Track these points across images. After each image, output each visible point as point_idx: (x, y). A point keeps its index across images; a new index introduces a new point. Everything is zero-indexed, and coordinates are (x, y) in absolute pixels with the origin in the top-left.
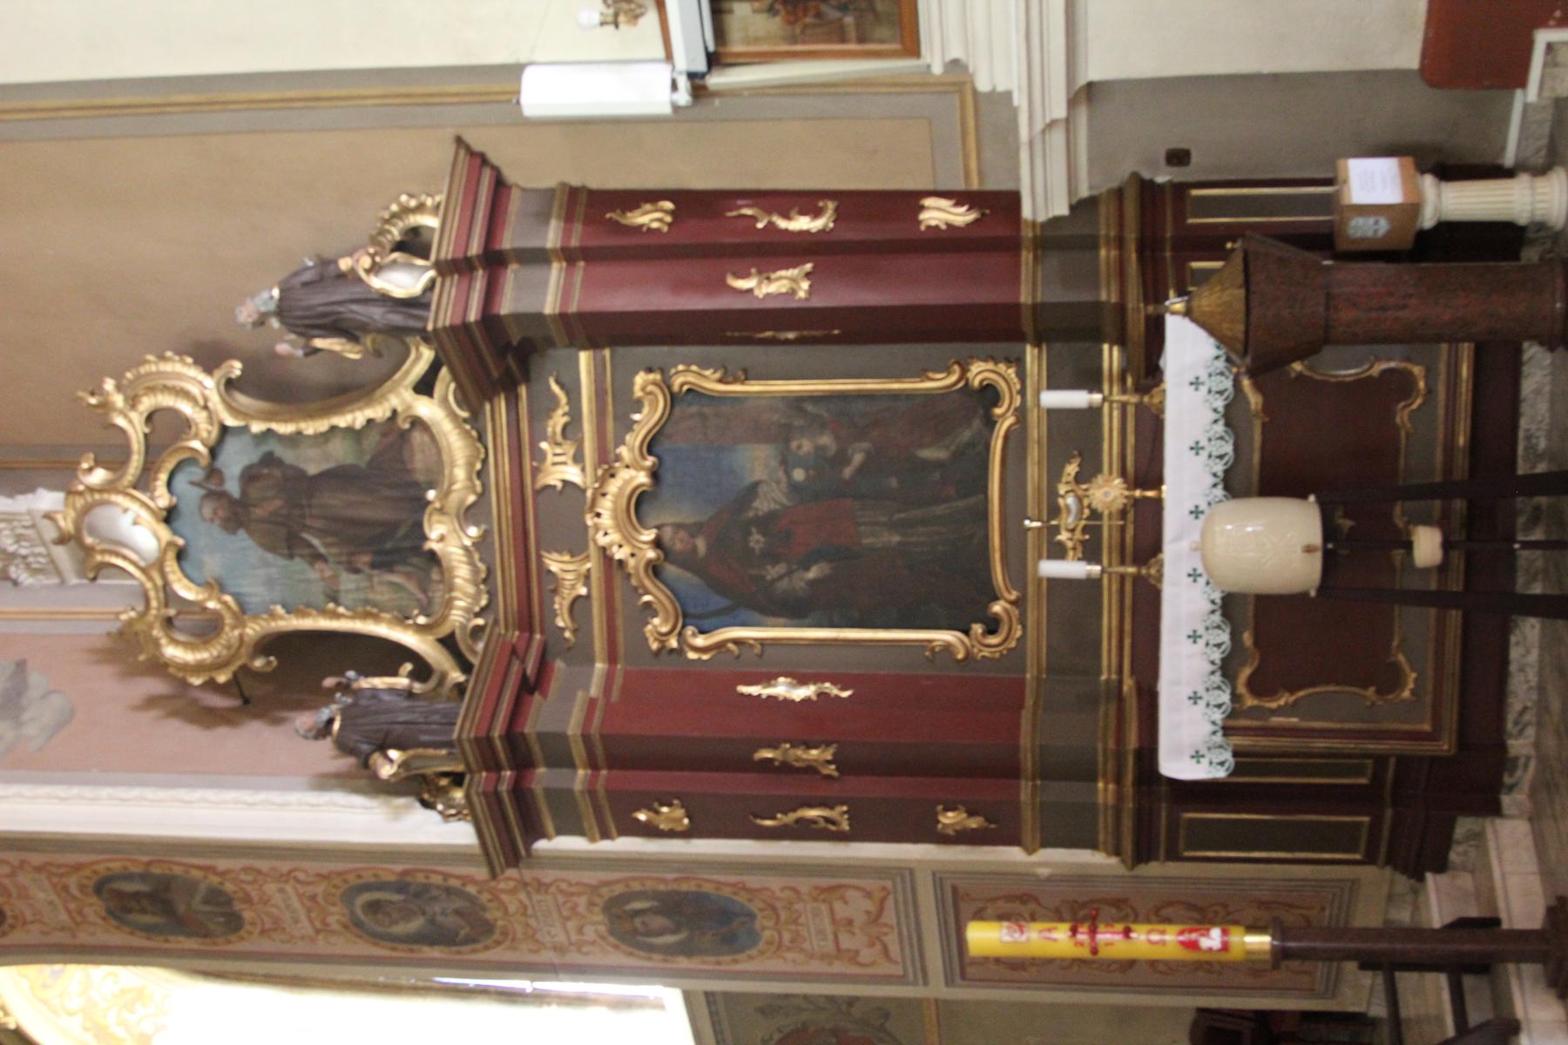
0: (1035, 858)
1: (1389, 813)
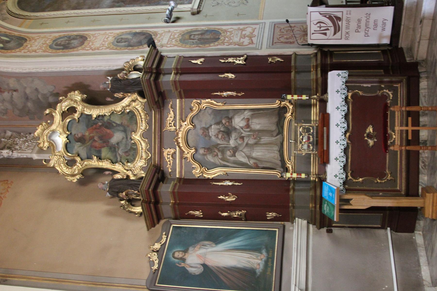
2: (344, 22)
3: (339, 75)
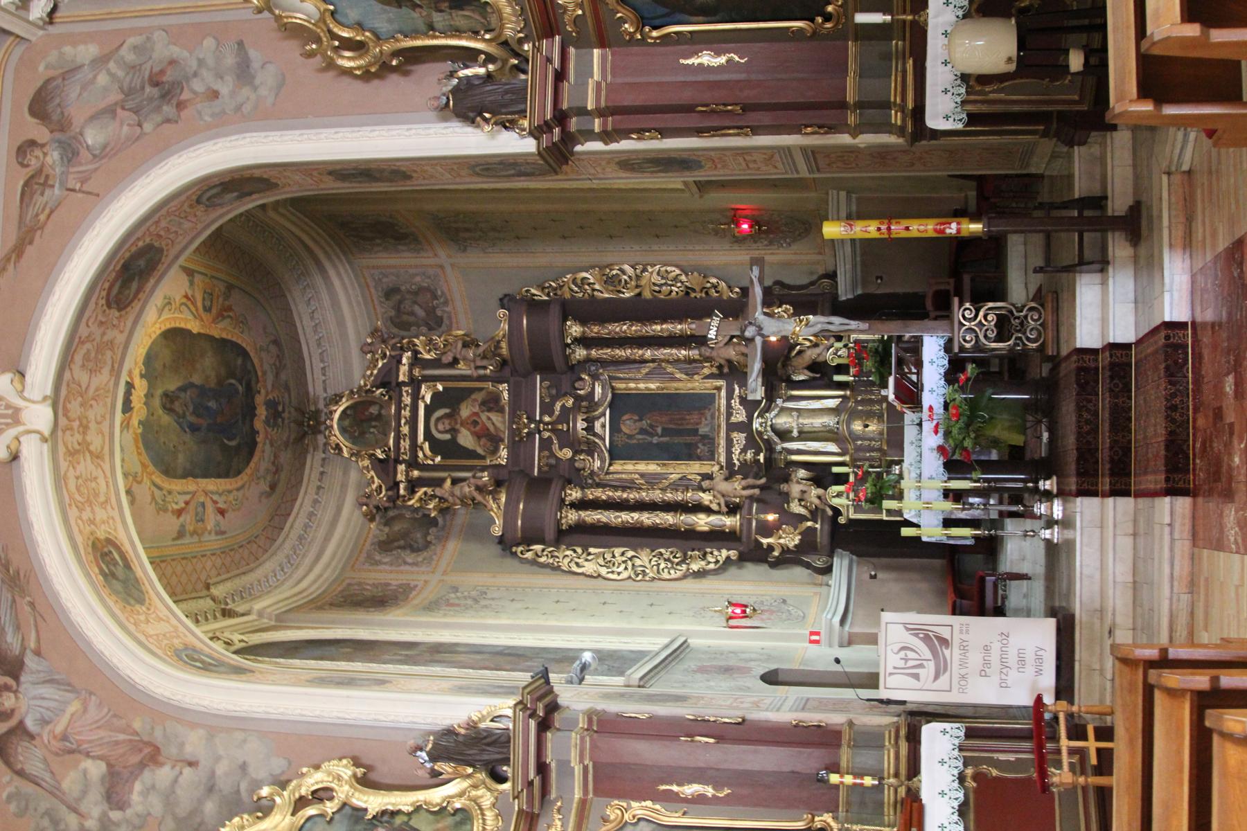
0: (857, 141)
1: (1055, 126)
2: (956, 651)
3: (944, 732)
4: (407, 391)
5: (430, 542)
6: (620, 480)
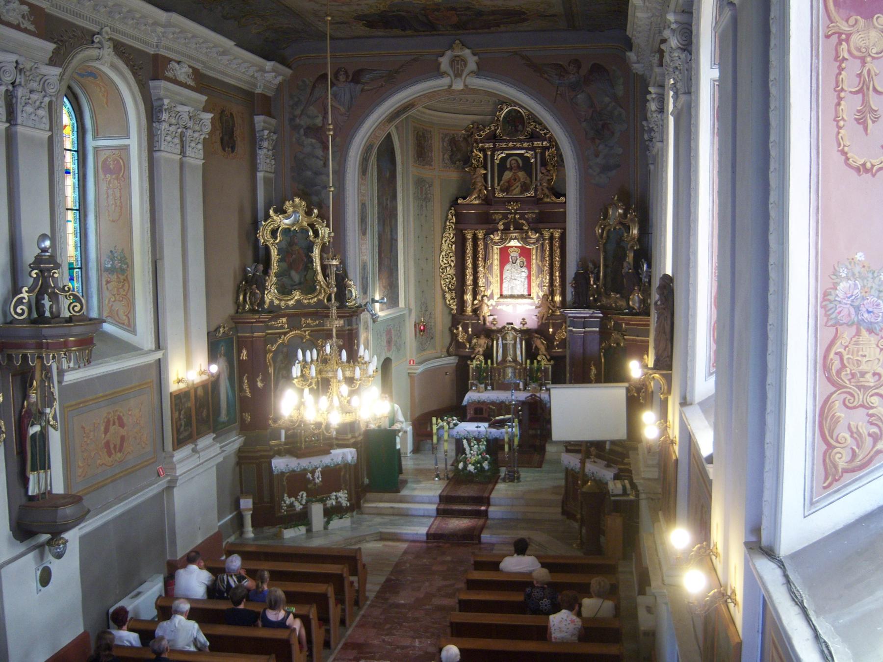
4: (529, 145)
5: (455, 164)
6: (489, 253)
